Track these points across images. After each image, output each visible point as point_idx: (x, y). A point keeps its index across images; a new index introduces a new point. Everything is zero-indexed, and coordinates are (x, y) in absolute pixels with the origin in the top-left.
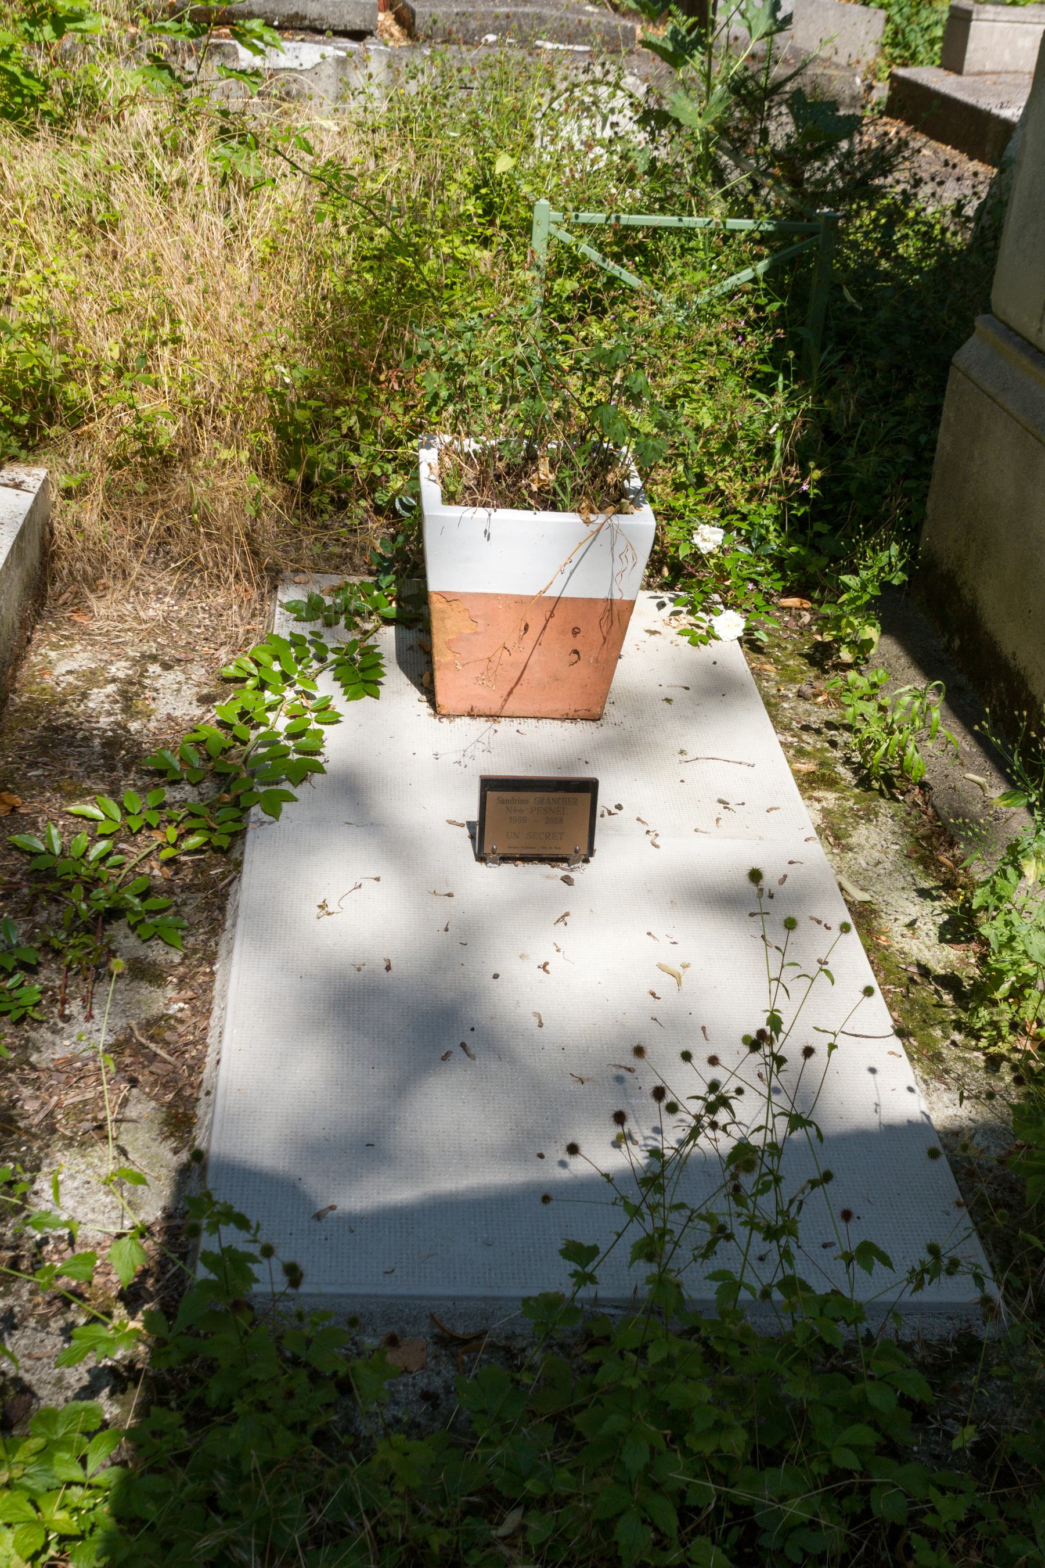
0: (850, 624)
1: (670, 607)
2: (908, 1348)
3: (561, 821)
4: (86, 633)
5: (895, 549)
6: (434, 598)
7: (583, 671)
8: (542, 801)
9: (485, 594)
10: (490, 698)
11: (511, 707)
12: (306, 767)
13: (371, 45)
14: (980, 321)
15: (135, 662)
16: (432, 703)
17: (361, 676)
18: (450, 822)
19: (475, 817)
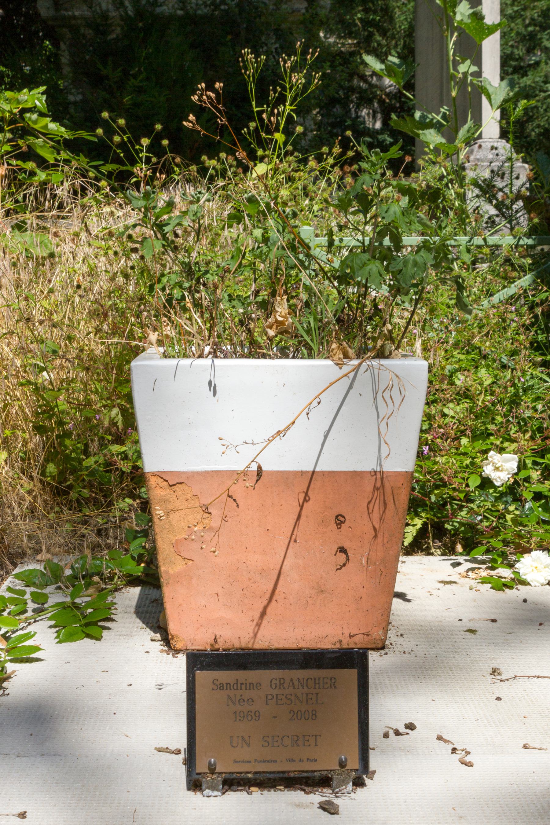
3: (314, 715)
6: (153, 482)
8: (281, 684)
9: (217, 473)
16: (167, 640)
18: (160, 750)
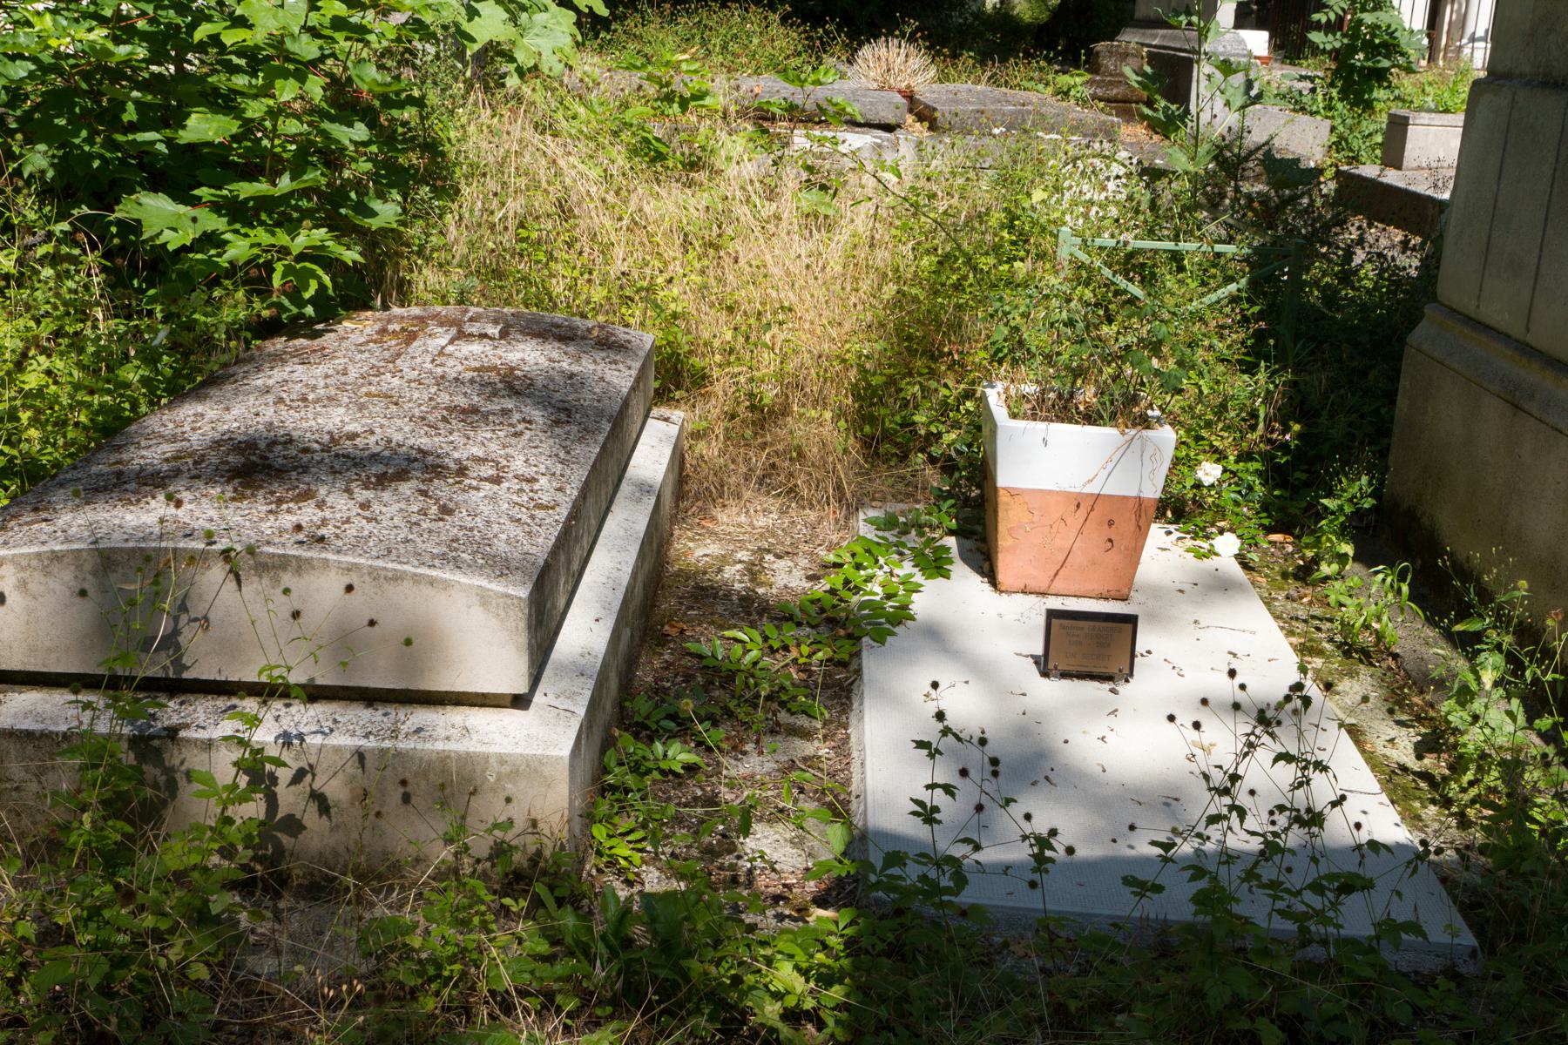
0: (1329, 540)
1: (1177, 535)
2: (1406, 975)
4: (712, 533)
5: (1364, 479)
6: (1001, 492)
7: (1115, 557)
10: (1040, 580)
11: (1058, 586)
12: (902, 615)
13: (900, 134)
14: (1428, 310)
15: (754, 552)
17: (936, 566)
19: (1039, 651)
